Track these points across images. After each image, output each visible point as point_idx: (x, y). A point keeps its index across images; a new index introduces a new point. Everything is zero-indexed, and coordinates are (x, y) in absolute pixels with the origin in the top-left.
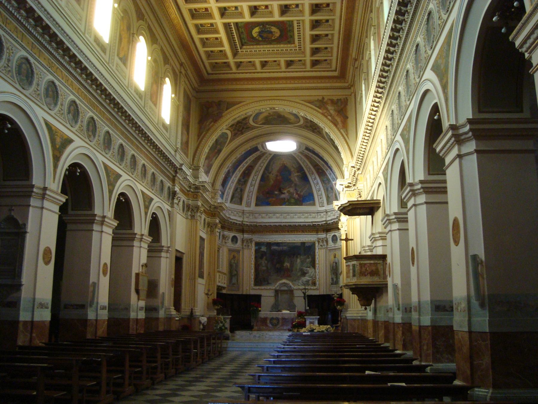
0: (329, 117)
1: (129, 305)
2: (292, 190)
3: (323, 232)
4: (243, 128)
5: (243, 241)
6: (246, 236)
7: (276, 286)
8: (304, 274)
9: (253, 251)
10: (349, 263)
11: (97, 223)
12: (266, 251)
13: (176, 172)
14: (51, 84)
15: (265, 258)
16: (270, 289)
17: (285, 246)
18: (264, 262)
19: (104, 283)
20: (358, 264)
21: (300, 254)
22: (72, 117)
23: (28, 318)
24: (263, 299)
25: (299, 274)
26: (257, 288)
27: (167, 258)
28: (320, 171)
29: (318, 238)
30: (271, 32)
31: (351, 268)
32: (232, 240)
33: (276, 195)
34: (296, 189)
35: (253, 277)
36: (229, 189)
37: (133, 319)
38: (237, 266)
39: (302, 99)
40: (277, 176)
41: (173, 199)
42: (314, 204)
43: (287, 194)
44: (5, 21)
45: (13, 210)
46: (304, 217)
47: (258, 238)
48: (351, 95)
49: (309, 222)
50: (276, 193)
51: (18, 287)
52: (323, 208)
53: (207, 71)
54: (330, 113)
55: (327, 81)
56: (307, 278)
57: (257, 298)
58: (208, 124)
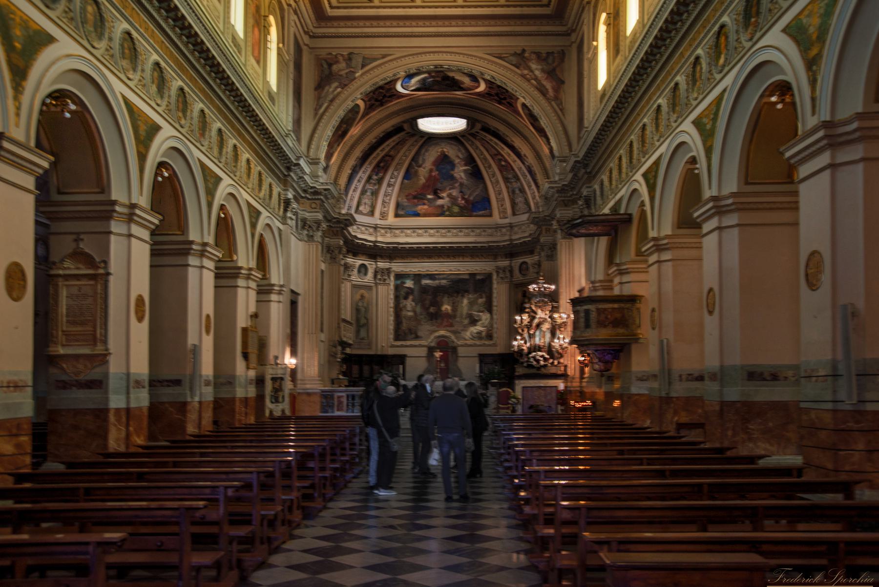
0: (533, 82)
1: (234, 377)
2: (455, 193)
3: (506, 258)
4: (385, 96)
5: (376, 273)
6: (381, 264)
7: (430, 340)
8: (474, 322)
9: (392, 287)
10: (578, 308)
11: (194, 255)
12: (412, 286)
13: (289, 169)
14: (127, 36)
15: (411, 297)
17: (444, 279)
18: (409, 304)
19: (208, 343)
20: (594, 309)
21: (467, 291)
22: (156, 89)
23: (122, 405)
24: (408, 361)
25: (466, 322)
27: (280, 302)
29: (496, 267)
31: (582, 315)
32: (359, 272)
33: (429, 200)
34: (461, 192)
35: (392, 327)
36: (354, 191)
37: (240, 399)
38: (367, 309)
39: (489, 52)
40: (431, 171)
42: (490, 215)
43: (447, 199)
45: (82, 240)
46: (474, 234)
47: (398, 267)
48: (570, 46)
49: (484, 243)
50: (429, 197)
51: (103, 359)
52: (507, 221)
54: (535, 75)
55: (499, 22)
56: (478, 328)
57: (401, 359)
58: (331, 90)
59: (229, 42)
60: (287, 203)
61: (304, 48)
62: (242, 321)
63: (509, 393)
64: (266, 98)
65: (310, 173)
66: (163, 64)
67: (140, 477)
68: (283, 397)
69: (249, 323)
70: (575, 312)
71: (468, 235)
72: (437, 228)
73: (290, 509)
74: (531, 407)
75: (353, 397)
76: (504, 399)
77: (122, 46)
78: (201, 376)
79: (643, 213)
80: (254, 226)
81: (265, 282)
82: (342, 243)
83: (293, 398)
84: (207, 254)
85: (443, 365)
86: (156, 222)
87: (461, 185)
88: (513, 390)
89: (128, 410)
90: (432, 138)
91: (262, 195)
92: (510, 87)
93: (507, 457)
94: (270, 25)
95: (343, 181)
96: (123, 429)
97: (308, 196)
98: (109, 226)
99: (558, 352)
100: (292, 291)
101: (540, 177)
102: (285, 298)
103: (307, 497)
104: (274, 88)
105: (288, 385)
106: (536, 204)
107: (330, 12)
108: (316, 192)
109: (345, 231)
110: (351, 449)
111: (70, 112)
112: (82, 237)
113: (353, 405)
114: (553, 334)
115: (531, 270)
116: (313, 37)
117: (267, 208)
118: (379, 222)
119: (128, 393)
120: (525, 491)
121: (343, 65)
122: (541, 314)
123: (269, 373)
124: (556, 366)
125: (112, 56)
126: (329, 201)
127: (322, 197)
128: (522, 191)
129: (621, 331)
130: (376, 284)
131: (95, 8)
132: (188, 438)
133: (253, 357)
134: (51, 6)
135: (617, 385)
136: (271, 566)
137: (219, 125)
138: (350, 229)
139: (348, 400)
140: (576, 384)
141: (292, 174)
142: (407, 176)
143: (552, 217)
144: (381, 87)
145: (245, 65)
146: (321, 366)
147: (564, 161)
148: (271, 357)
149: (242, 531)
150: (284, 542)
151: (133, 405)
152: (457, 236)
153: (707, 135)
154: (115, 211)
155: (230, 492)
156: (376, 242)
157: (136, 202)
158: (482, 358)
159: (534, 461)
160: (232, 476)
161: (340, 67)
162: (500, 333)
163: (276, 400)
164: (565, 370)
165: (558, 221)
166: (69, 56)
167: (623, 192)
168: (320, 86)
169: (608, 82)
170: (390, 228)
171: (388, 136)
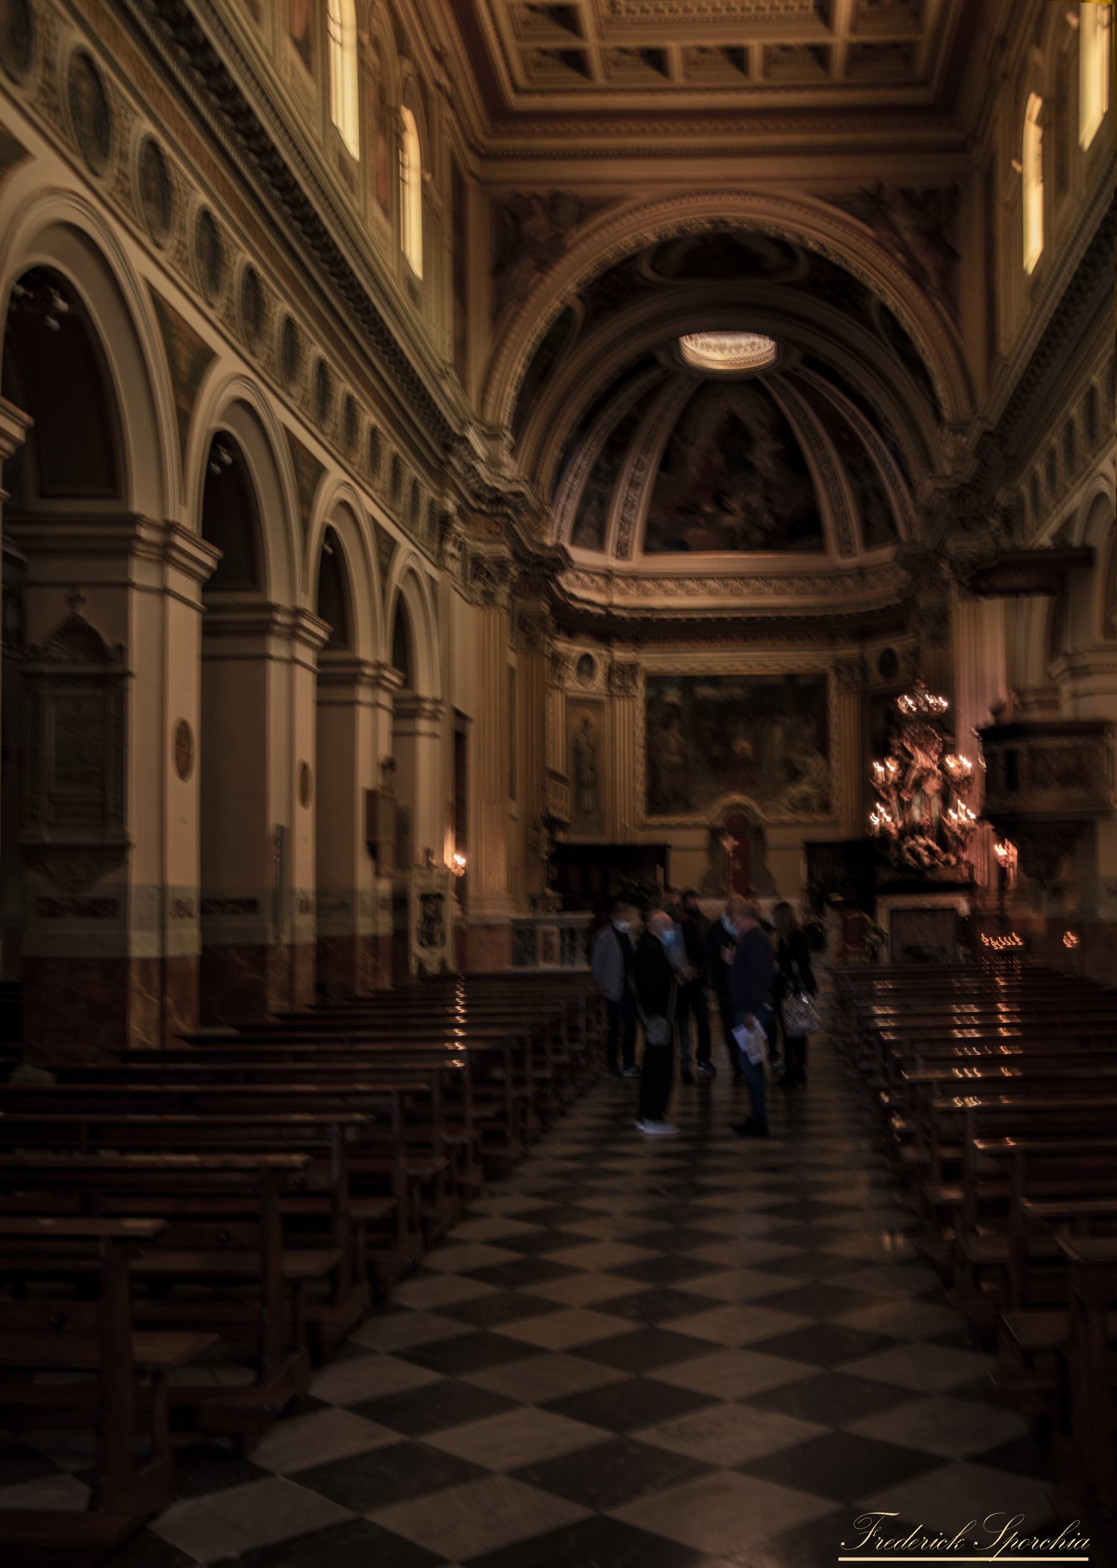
1: (351, 893)
2: (755, 500)
6: (621, 655)
8: (794, 774)
9: (640, 703)
10: (996, 748)
11: (279, 635)
16: (696, 826)
18: (673, 737)
19: (305, 820)
24: (674, 857)
26: (663, 820)
32: (580, 669)
35: (641, 788)
41: (442, 539)
42: (820, 548)
45: (83, 600)
52: (850, 562)
53: (512, 78)
57: (659, 854)
59: (331, 168)
61: (469, 181)
62: (366, 777)
63: (864, 920)
64: (400, 290)
65: (487, 458)
67: (187, 1102)
68: (443, 936)
69: (380, 781)
70: (988, 756)
71: (780, 592)
72: (721, 577)
73: (461, 1162)
74: (908, 950)
75: (572, 933)
76: (854, 934)
77: (143, 172)
78: (292, 891)
80: (385, 571)
81: (406, 693)
82: (545, 608)
83: (461, 935)
84: (302, 633)
85: (738, 866)
88: (873, 915)
89: (163, 962)
92: (856, 266)
93: (866, 1050)
94: (404, 129)
95: (546, 474)
96: (155, 1001)
97: (484, 507)
98: (126, 571)
99: (955, 837)
100: (459, 715)
101: (914, 466)
102: (443, 728)
103: (492, 1136)
104: (417, 269)
105: (451, 910)
107: (517, 102)
108: (498, 499)
109: (553, 586)
110: (573, 1040)
112: (83, 593)
113: (573, 950)
114: (947, 801)
115: (902, 664)
116: (485, 156)
117: (408, 533)
118: (614, 563)
119: (163, 927)
120: (904, 1117)
122: (922, 760)
123: (418, 883)
124: (953, 867)
125: (127, 195)
126: (523, 519)
127: (509, 511)
128: (881, 496)
129: (1076, 794)
130: (611, 696)
132: (271, 1020)
133: (387, 853)
134: (18, 76)
135: (1070, 905)
136: (430, 1272)
137: (320, 351)
138: (561, 579)
139: (563, 939)
140: (991, 902)
141: (454, 461)
142: (666, 465)
146: (511, 868)
148: (420, 853)
149: (374, 1208)
150: (452, 1227)
151: (172, 951)
152: (761, 593)
154: (139, 538)
155: (351, 1135)
156: (611, 605)
157: (177, 520)
158: (813, 850)
159: (920, 1061)
160: (352, 1101)
161: (536, 225)
162: (843, 794)
163: (429, 940)
164: (971, 875)
165: (952, 565)
166: (53, 191)
167: (1077, 499)
168: (499, 268)
169: (1044, 256)
170: (634, 577)
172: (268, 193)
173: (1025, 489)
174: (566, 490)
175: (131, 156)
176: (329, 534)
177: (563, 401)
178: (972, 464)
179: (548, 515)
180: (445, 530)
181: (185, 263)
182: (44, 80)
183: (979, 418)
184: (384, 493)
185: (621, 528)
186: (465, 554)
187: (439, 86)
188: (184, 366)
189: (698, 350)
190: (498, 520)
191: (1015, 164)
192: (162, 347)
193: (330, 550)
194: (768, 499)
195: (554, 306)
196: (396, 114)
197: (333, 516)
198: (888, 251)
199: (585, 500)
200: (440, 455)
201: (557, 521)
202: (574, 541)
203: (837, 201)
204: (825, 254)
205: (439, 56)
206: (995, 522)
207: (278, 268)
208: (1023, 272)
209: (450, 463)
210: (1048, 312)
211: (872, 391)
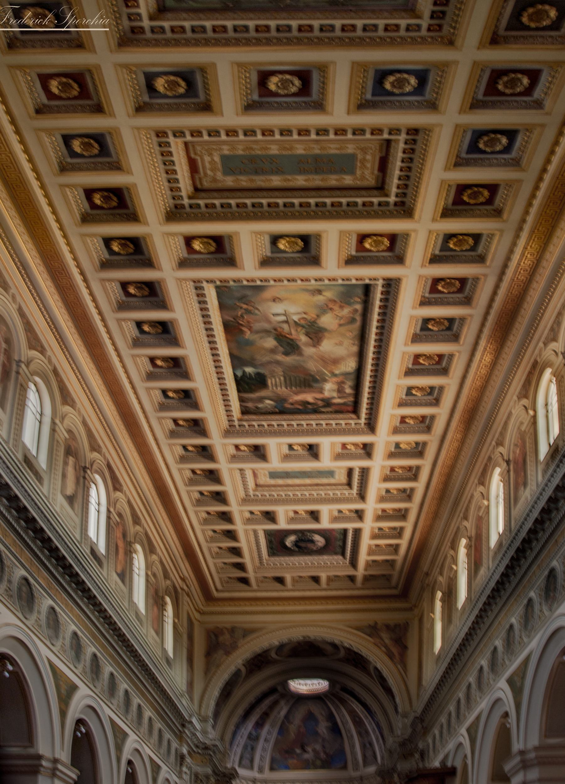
2: (318, 747)
28: (357, 719)
30: (312, 541)
41: (181, 765)
44: (5, 535)
54: (385, 643)
59: (133, 617)
60: (182, 757)
61: (196, 623)
66: (79, 633)
77: (48, 618)
79: (465, 766)
86: (74, 776)
87: (324, 740)
90: (301, 698)
91: (162, 751)
92: (364, 652)
94: (166, 604)
97: (200, 751)
101: (386, 732)
106: (382, 758)
108: (206, 748)
111: (9, 672)
116: (202, 613)
121: (227, 636)
125: (40, 626)
127: (211, 753)
128: (371, 744)
131: (28, 588)
137: (126, 686)
141: (186, 731)
143: (394, 769)
144: (259, 655)
145: (147, 637)
147: (406, 717)
153: (517, 690)
154: (42, 766)
161: (225, 638)
165: (399, 775)
166: (7, 625)
168: (209, 654)
169: (442, 648)
171: (264, 696)
172: (103, 626)
173: (430, 741)
174: (237, 743)
175: (42, 612)
176: (130, 763)
177: (236, 706)
178: (409, 730)
179: (228, 754)
180: (182, 761)
181: (65, 651)
182: (7, 586)
183: (414, 712)
184: (155, 745)
185: (261, 760)
186: (191, 771)
187: (182, 589)
188: (63, 691)
189: (296, 686)
190: (206, 757)
191: (431, 614)
192: (530, 664)
193: (130, 771)
194: (324, 747)
195: (232, 669)
196: (163, 598)
197: (131, 755)
198: (378, 647)
199: (245, 747)
200: (180, 729)
201: (233, 756)
202: (240, 765)
203: (358, 629)
204: (352, 648)
205: (183, 579)
206: (417, 756)
207: (106, 653)
208: (434, 654)
209: (184, 731)
210: (443, 669)
211: (369, 701)
